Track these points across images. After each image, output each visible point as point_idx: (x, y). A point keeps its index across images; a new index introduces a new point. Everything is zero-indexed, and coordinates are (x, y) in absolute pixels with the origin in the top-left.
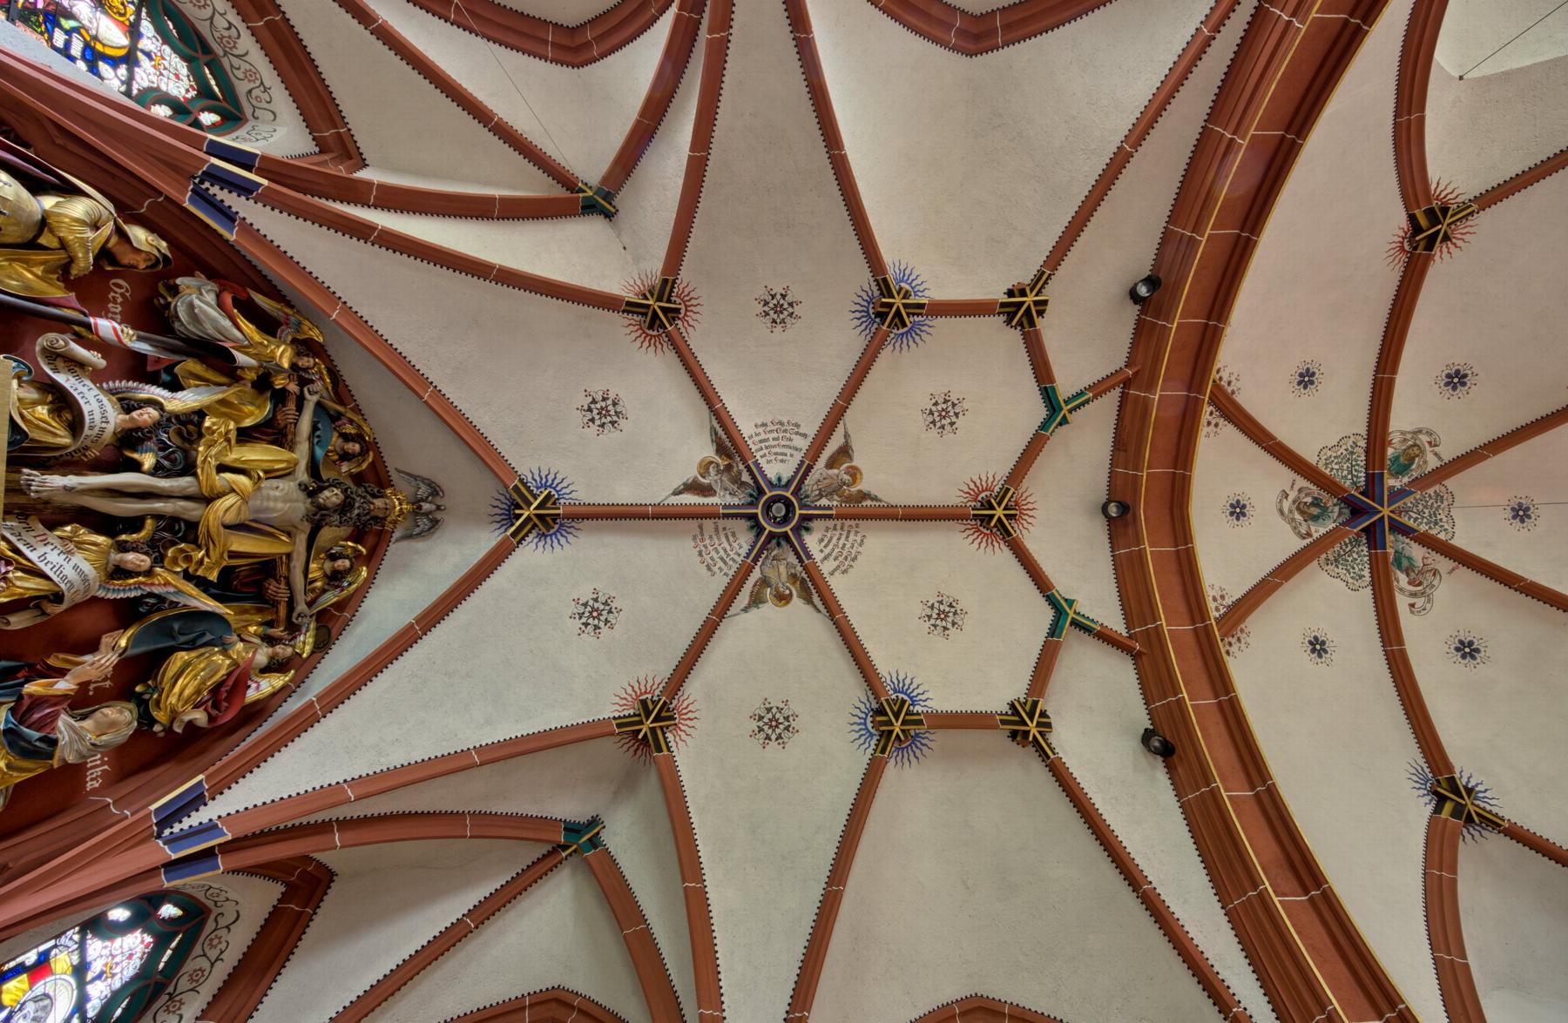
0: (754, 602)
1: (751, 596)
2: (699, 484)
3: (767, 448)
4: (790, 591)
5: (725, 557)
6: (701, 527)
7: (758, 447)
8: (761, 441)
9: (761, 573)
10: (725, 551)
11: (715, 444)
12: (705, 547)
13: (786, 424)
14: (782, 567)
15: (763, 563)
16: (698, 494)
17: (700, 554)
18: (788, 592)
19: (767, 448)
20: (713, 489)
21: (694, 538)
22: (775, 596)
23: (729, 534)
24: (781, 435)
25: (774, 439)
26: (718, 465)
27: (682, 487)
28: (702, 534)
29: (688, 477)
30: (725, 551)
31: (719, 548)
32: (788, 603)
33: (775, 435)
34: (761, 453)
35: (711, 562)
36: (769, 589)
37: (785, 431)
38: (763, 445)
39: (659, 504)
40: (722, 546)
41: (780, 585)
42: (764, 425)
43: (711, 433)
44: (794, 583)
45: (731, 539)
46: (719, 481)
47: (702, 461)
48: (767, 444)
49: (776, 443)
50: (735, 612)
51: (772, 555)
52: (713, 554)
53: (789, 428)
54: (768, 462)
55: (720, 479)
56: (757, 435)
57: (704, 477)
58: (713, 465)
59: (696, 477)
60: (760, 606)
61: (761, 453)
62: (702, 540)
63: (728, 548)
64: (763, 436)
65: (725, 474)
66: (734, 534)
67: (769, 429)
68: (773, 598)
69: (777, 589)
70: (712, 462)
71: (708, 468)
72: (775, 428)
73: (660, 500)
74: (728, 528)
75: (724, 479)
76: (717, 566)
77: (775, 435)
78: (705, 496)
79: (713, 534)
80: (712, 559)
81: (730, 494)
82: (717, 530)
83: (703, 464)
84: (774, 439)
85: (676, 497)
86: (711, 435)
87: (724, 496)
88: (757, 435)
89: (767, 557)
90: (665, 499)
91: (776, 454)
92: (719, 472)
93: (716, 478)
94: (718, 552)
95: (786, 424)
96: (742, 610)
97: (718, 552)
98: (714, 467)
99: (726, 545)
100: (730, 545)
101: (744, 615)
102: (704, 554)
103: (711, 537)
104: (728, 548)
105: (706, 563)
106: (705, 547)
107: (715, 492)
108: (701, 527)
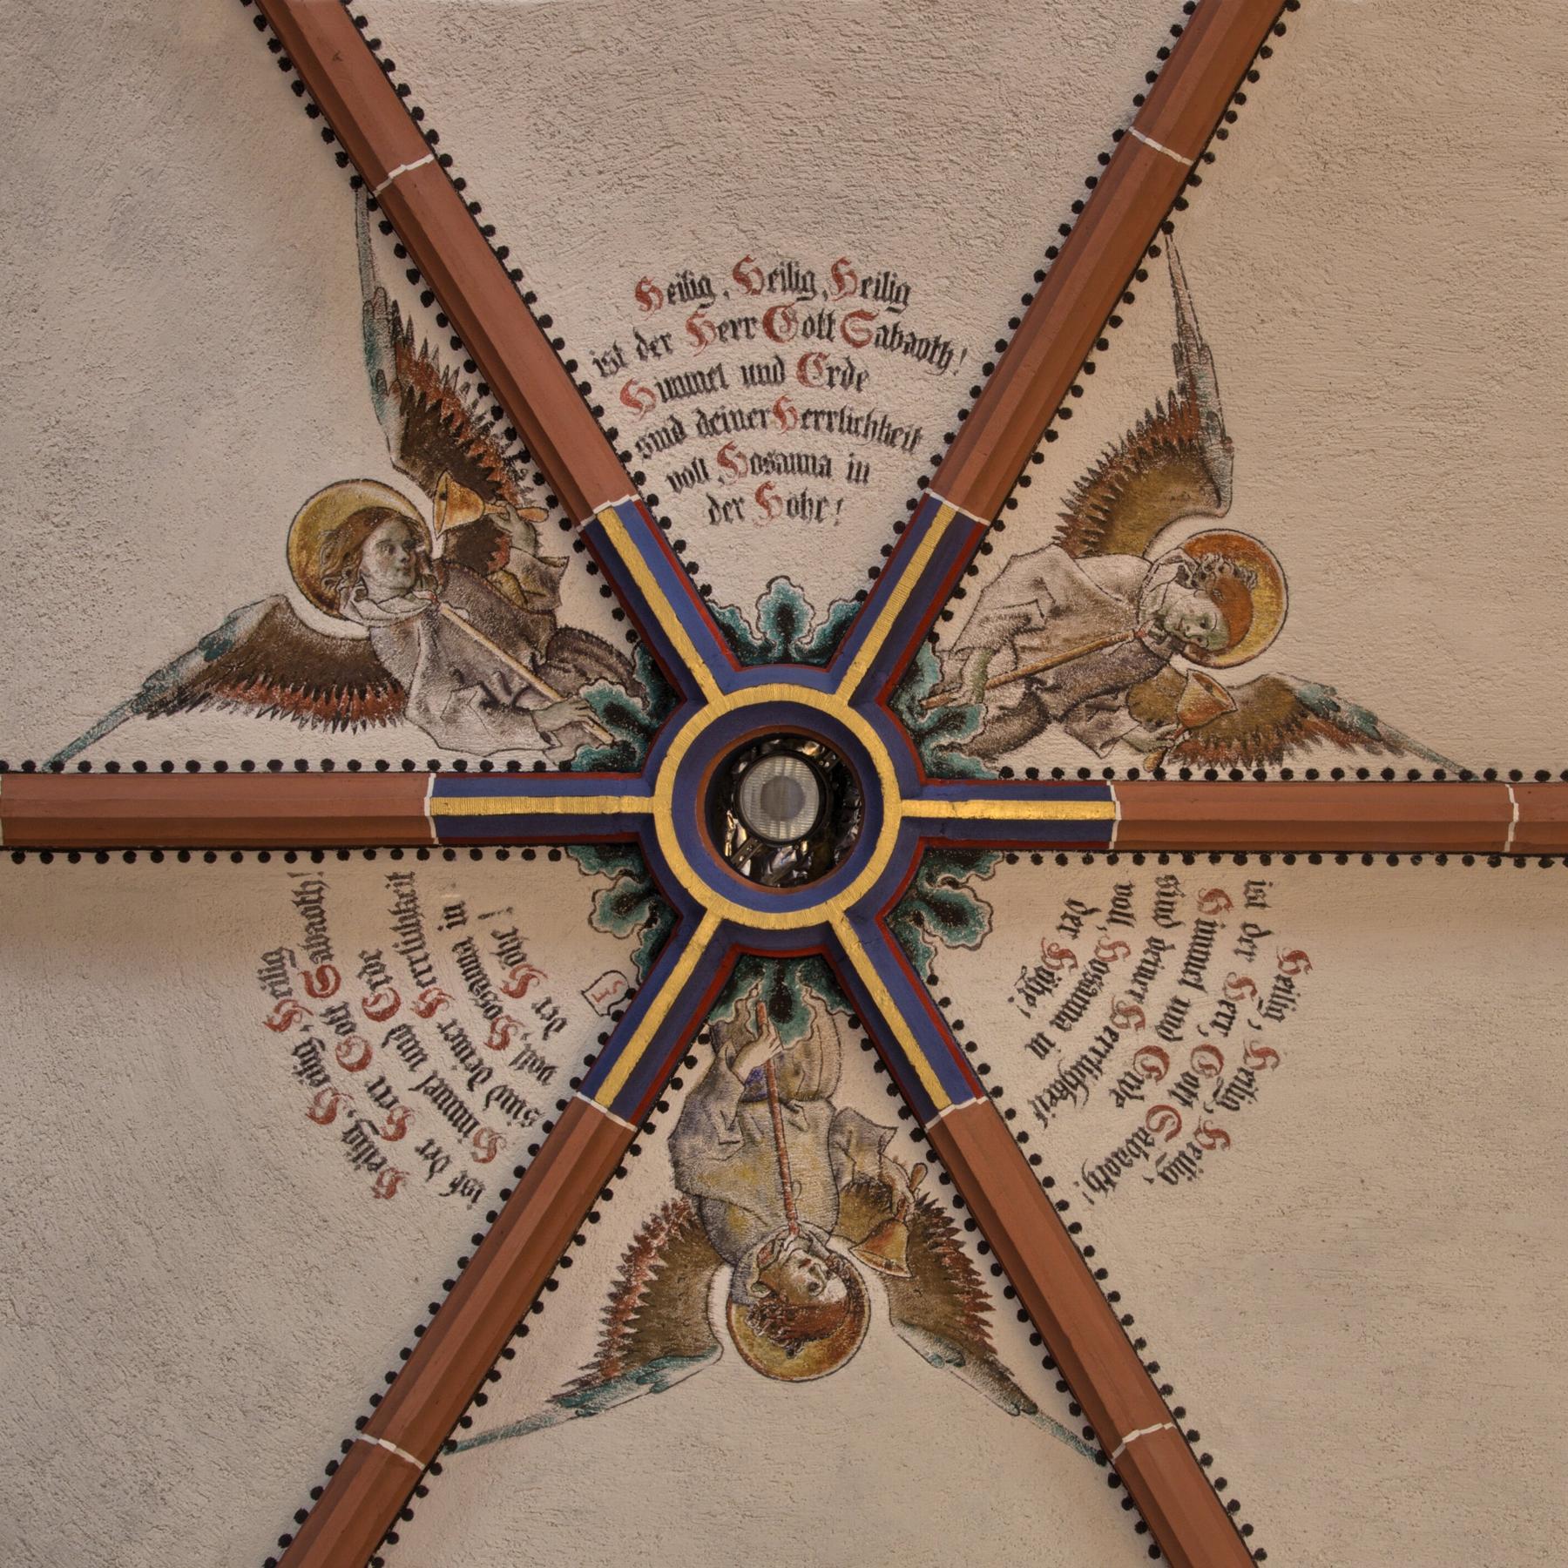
0: (636, 1351)
1: (615, 1315)
2: (296, 643)
3: (707, 425)
4: (852, 1283)
5: (457, 1080)
6: (311, 904)
7: (657, 418)
8: (671, 389)
9: (679, 1181)
10: (461, 1047)
11: (392, 404)
12: (340, 1021)
13: (823, 282)
14: (806, 1138)
15: (687, 1122)
16: (297, 710)
17: (309, 1063)
18: (836, 1290)
19: (707, 425)
20: (388, 675)
21: (274, 970)
22: (759, 1314)
23: (486, 948)
24: (792, 351)
25: (751, 375)
26: (413, 531)
27: (197, 662)
28: (320, 947)
29: (235, 601)
30: (461, 1047)
31: (426, 1032)
32: (836, 1355)
33: (759, 350)
34: (677, 458)
35: (378, 1116)
36: (724, 1276)
37: (820, 326)
38: (685, 409)
39: (57, 766)
40: (442, 1015)
41: (794, 1249)
42: (692, 288)
43: (369, 335)
44: (874, 1239)
45: (497, 974)
46: (418, 625)
47: (318, 506)
48: (710, 404)
49: (762, 396)
50: (520, 1413)
51: (744, 1070)
52: (389, 1062)
53: (840, 308)
54: (718, 511)
55: (429, 615)
56: (649, 348)
57: (329, 605)
58: (380, 534)
59: (281, 605)
60: (672, 1374)
61: (677, 458)
62: (322, 983)
63: (478, 1031)
64: (685, 358)
65: (460, 586)
66: (511, 949)
67: (718, 313)
68: (744, 1325)
69: (771, 1277)
70: (374, 516)
71: (355, 552)
72: (757, 306)
73: (63, 744)
74: (472, 911)
75: (455, 614)
76: (415, 1138)
77: (759, 350)
78: (339, 719)
79: (387, 942)
80: (381, 1093)
81: (490, 703)
82: (408, 918)
83: (325, 525)
84: (751, 375)
85: (162, 720)
86: (371, 352)
87: (451, 718)
88: (649, 348)
89: (711, 1082)
90: (95, 736)
91: (763, 463)
92: (417, 570)
93: (401, 607)
94: (414, 1055)
95: (823, 282)
96: (562, 1400)
97: (414, 1055)
98: (388, 546)
99: (463, 1010)
100: (491, 1012)
101: (574, 1431)
102: (329, 1060)
103: (372, 964)
104: (478, 1031)
105: (342, 1123)
106: (340, 1021)
107: (399, 692)
108: (311, 904)
